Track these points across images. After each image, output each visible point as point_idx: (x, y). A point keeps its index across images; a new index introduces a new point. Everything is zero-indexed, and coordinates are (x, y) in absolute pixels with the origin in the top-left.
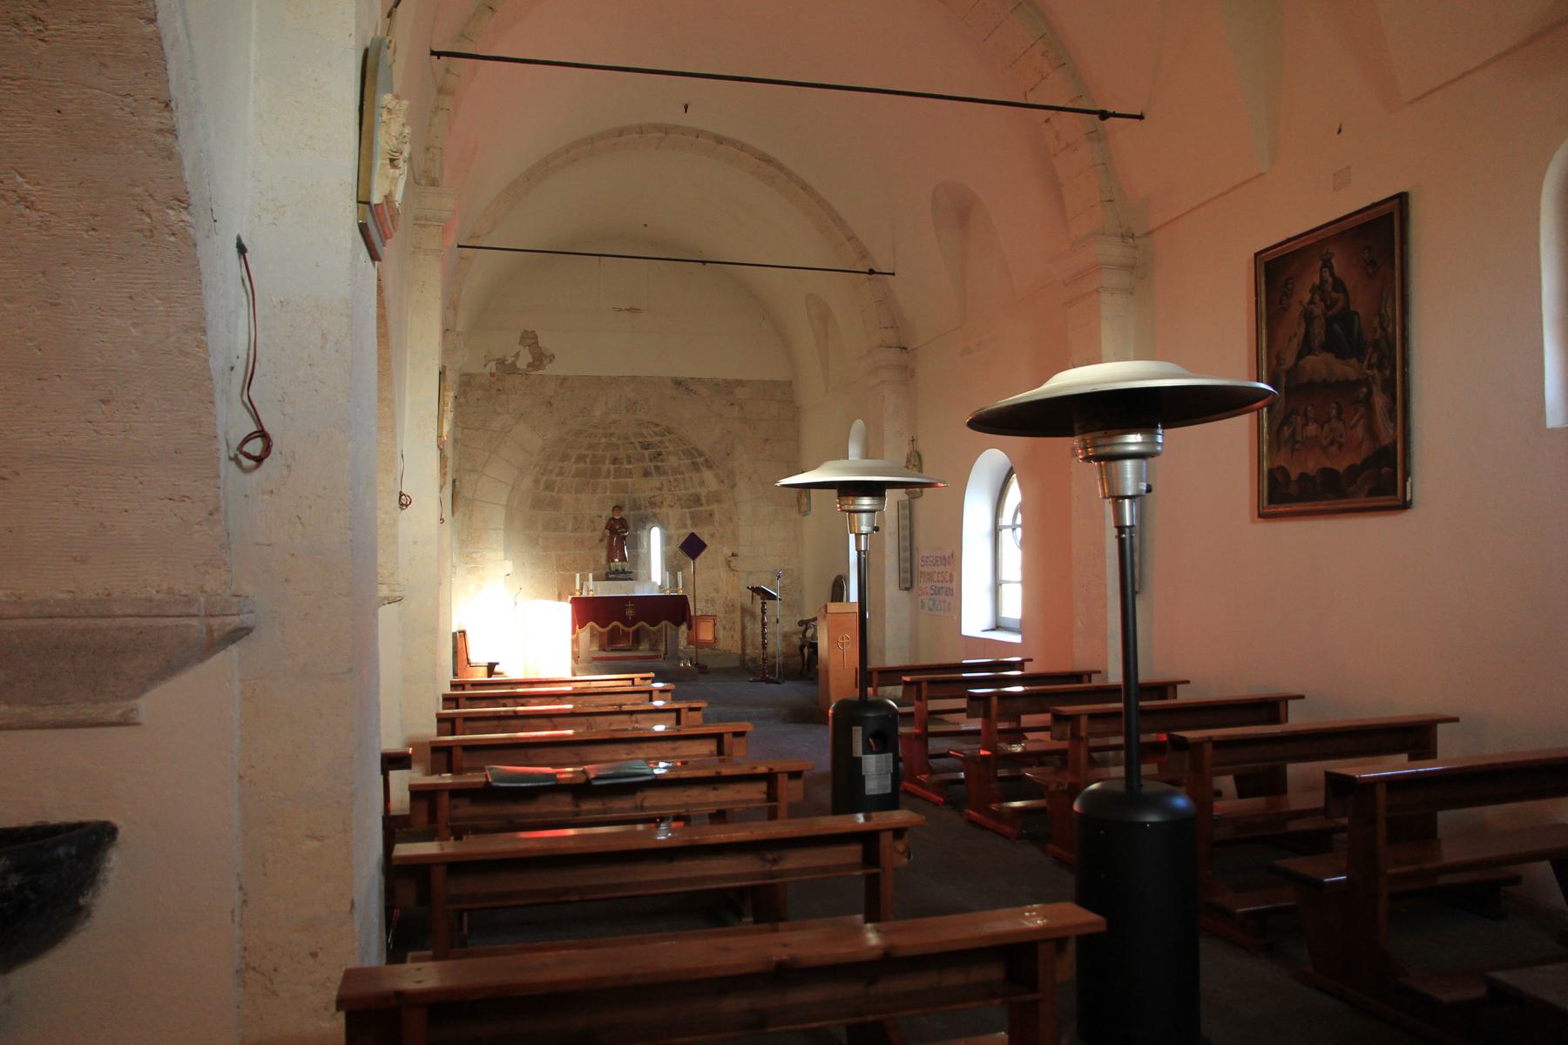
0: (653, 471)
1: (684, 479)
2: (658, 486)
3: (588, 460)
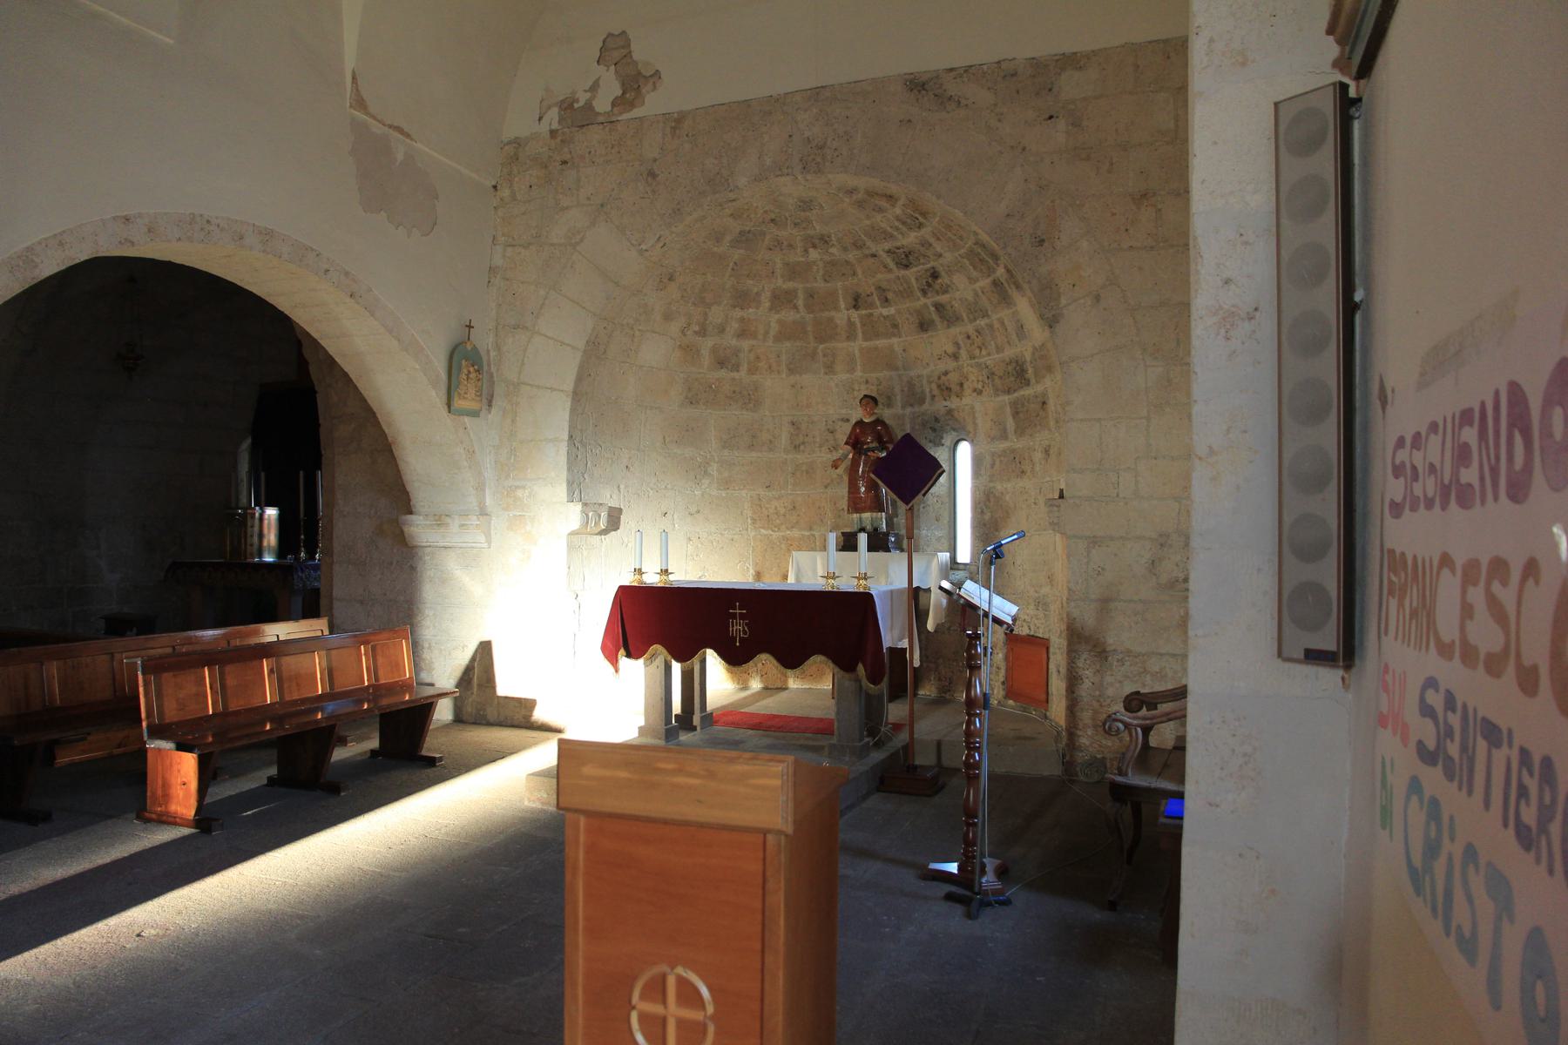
0: (935, 317)
1: (991, 326)
2: (950, 349)
3: (800, 303)
